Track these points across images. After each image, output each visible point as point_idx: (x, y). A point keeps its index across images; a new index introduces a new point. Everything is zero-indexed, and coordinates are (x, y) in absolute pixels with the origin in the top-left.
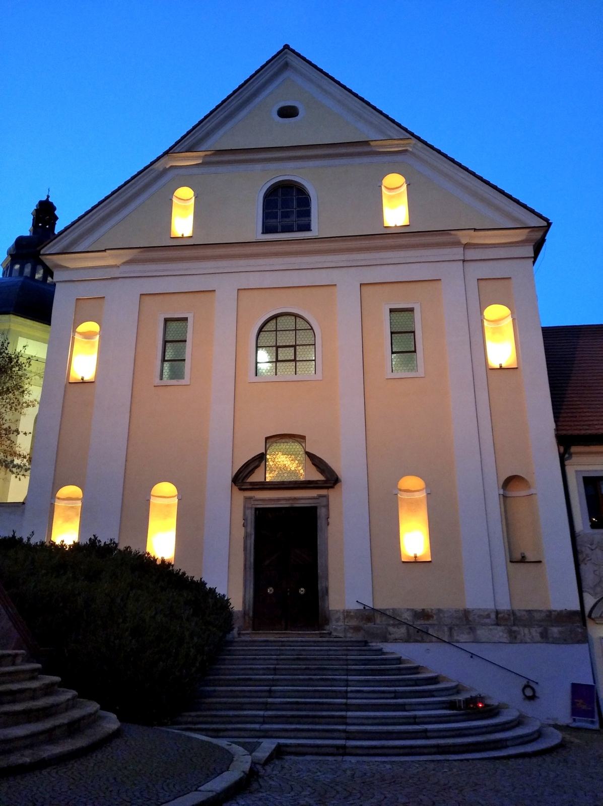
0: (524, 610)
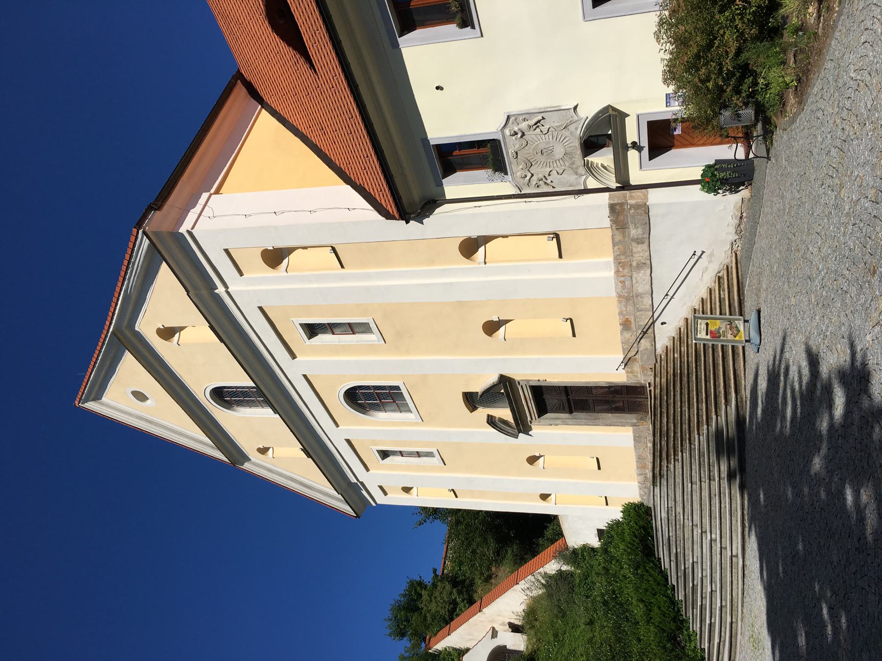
0: (613, 248)
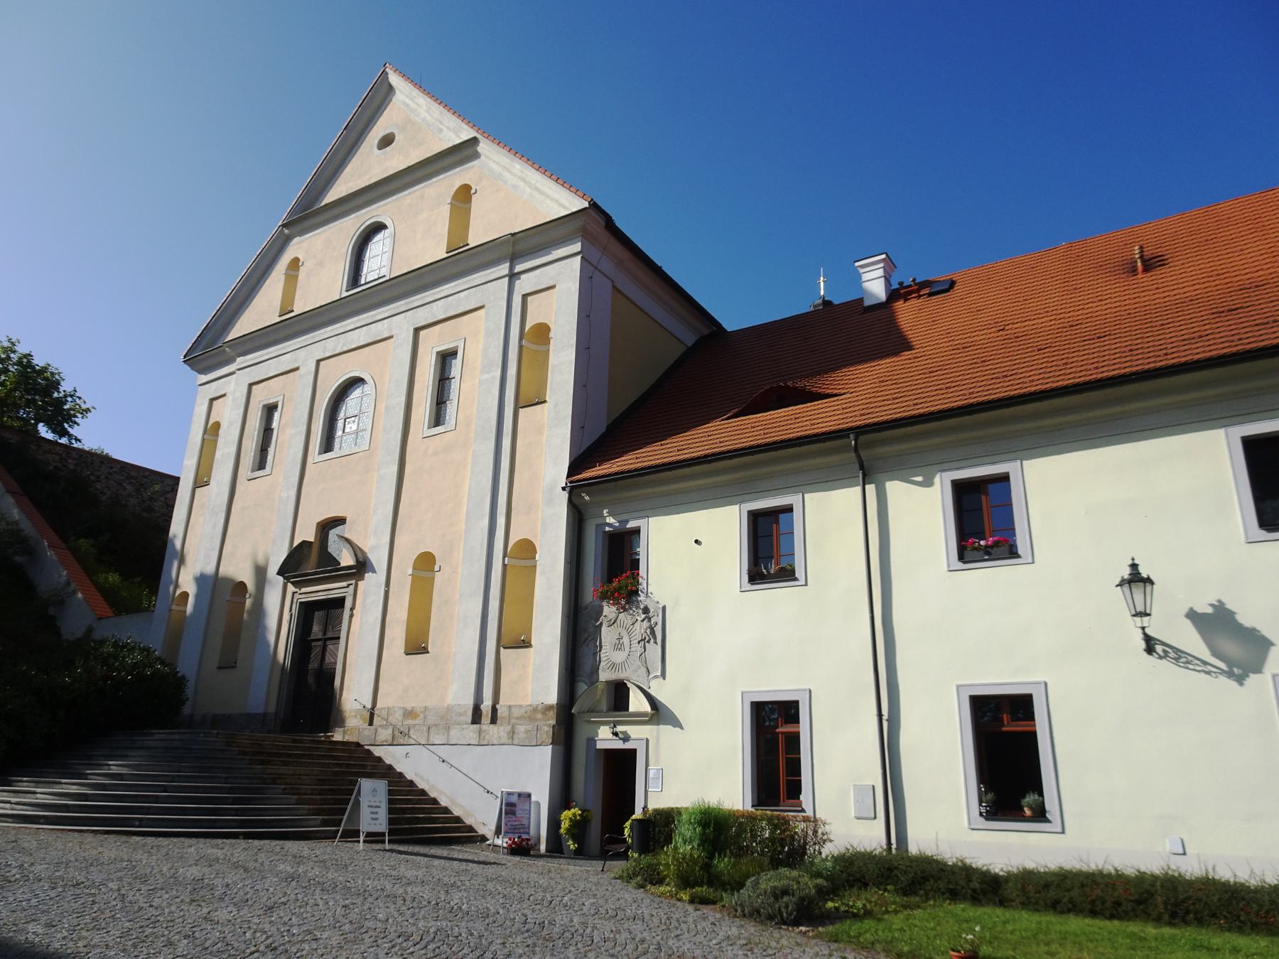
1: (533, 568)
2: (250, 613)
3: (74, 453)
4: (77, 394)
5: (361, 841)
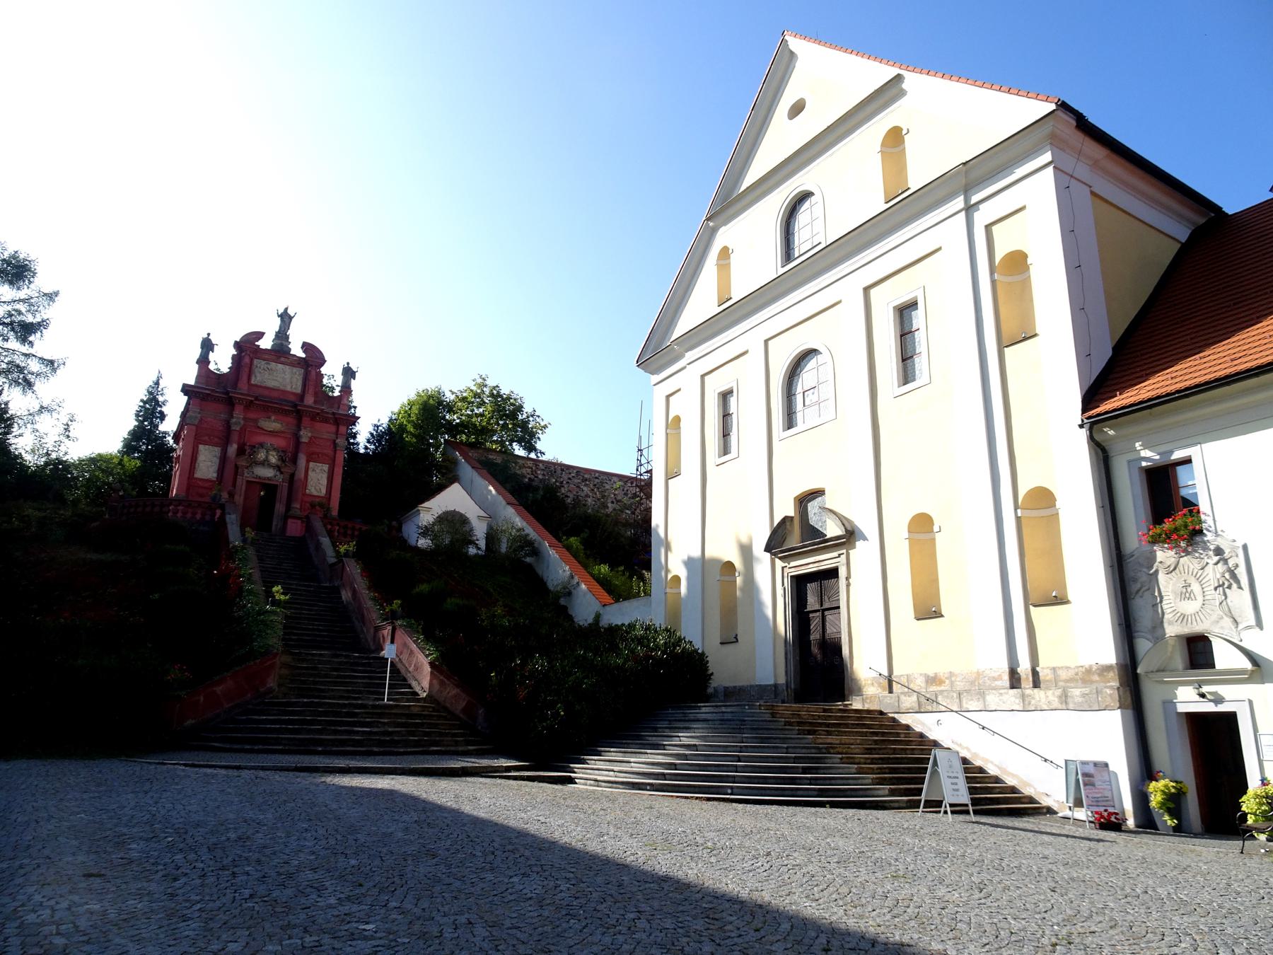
0: (1048, 668)
1: (1056, 516)
2: (742, 590)
3: (541, 465)
4: (536, 414)
5: (942, 812)
